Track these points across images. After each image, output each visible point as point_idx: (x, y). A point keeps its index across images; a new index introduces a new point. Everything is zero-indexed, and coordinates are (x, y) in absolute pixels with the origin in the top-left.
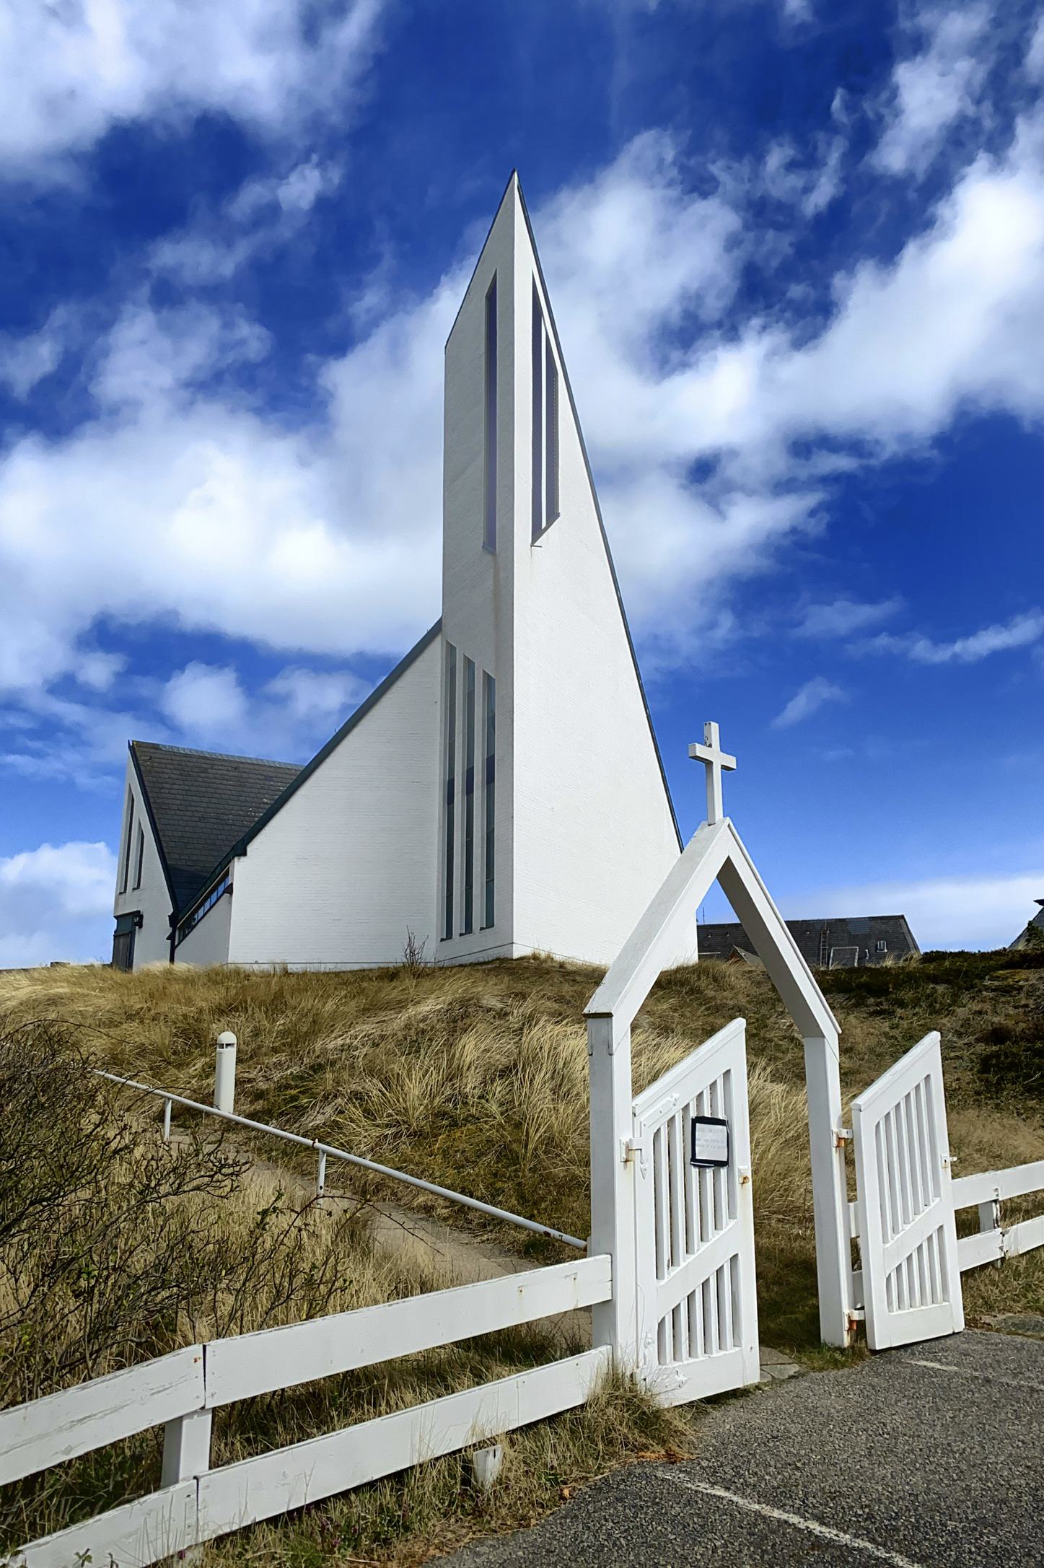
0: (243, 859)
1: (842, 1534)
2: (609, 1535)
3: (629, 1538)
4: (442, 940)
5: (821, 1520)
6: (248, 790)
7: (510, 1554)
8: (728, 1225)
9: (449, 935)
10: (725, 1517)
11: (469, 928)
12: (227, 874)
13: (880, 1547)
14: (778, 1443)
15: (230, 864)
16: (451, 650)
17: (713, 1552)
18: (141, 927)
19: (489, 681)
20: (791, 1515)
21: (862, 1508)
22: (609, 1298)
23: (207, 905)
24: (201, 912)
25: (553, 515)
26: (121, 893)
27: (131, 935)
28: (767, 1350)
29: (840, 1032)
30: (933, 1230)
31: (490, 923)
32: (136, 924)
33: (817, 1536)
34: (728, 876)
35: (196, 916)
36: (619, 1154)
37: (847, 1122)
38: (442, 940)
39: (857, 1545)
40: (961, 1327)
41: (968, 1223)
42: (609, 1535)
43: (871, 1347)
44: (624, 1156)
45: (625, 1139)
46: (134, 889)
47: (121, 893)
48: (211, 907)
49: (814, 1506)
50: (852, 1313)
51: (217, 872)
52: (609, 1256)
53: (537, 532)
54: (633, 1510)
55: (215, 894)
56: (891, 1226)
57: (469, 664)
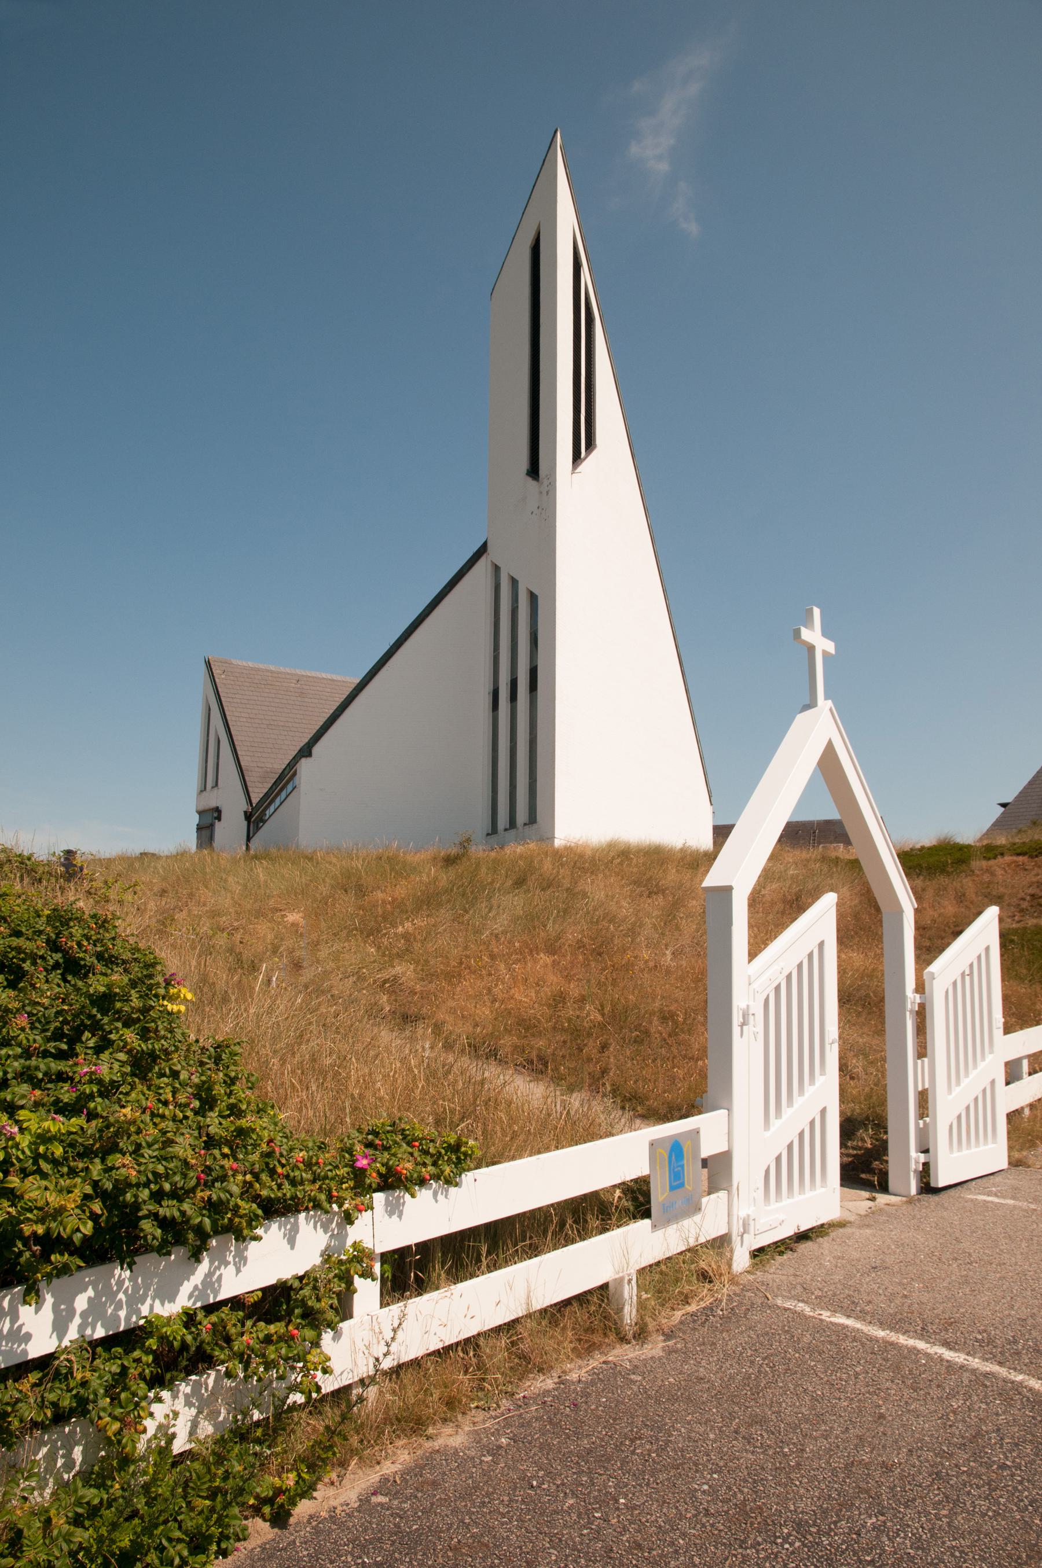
0: (309, 760)
1: (970, 1358)
2: (752, 1362)
3: (771, 1365)
4: (488, 834)
5: (946, 1344)
6: (310, 701)
7: (662, 1381)
8: (820, 1080)
9: (494, 830)
10: (855, 1344)
11: (512, 824)
12: (295, 774)
13: (1011, 1371)
14: (879, 1273)
15: (298, 765)
16: (497, 569)
17: (856, 1378)
18: (245, 812)
19: (533, 598)
20: (917, 1341)
21: (979, 1332)
22: (726, 1149)
23: (277, 802)
24: (272, 808)
25: (590, 444)
26: (201, 791)
27: (211, 827)
28: (846, 1189)
29: (916, 906)
30: (986, 1083)
31: (532, 819)
32: (216, 818)
33: (948, 1361)
34: (829, 763)
35: (267, 812)
36: (736, 1019)
37: (920, 988)
38: (488, 834)
39: (988, 1369)
40: (1004, 1164)
41: (1012, 1073)
42: (752, 1362)
43: (933, 1185)
44: (741, 1020)
45: (743, 1006)
46: (213, 787)
47: (201, 791)
48: (281, 804)
49: (934, 1332)
50: (919, 1157)
51: (286, 772)
52: (726, 1111)
53: (577, 458)
54: (767, 1338)
55: (284, 792)
56: (955, 1077)
57: (514, 582)
